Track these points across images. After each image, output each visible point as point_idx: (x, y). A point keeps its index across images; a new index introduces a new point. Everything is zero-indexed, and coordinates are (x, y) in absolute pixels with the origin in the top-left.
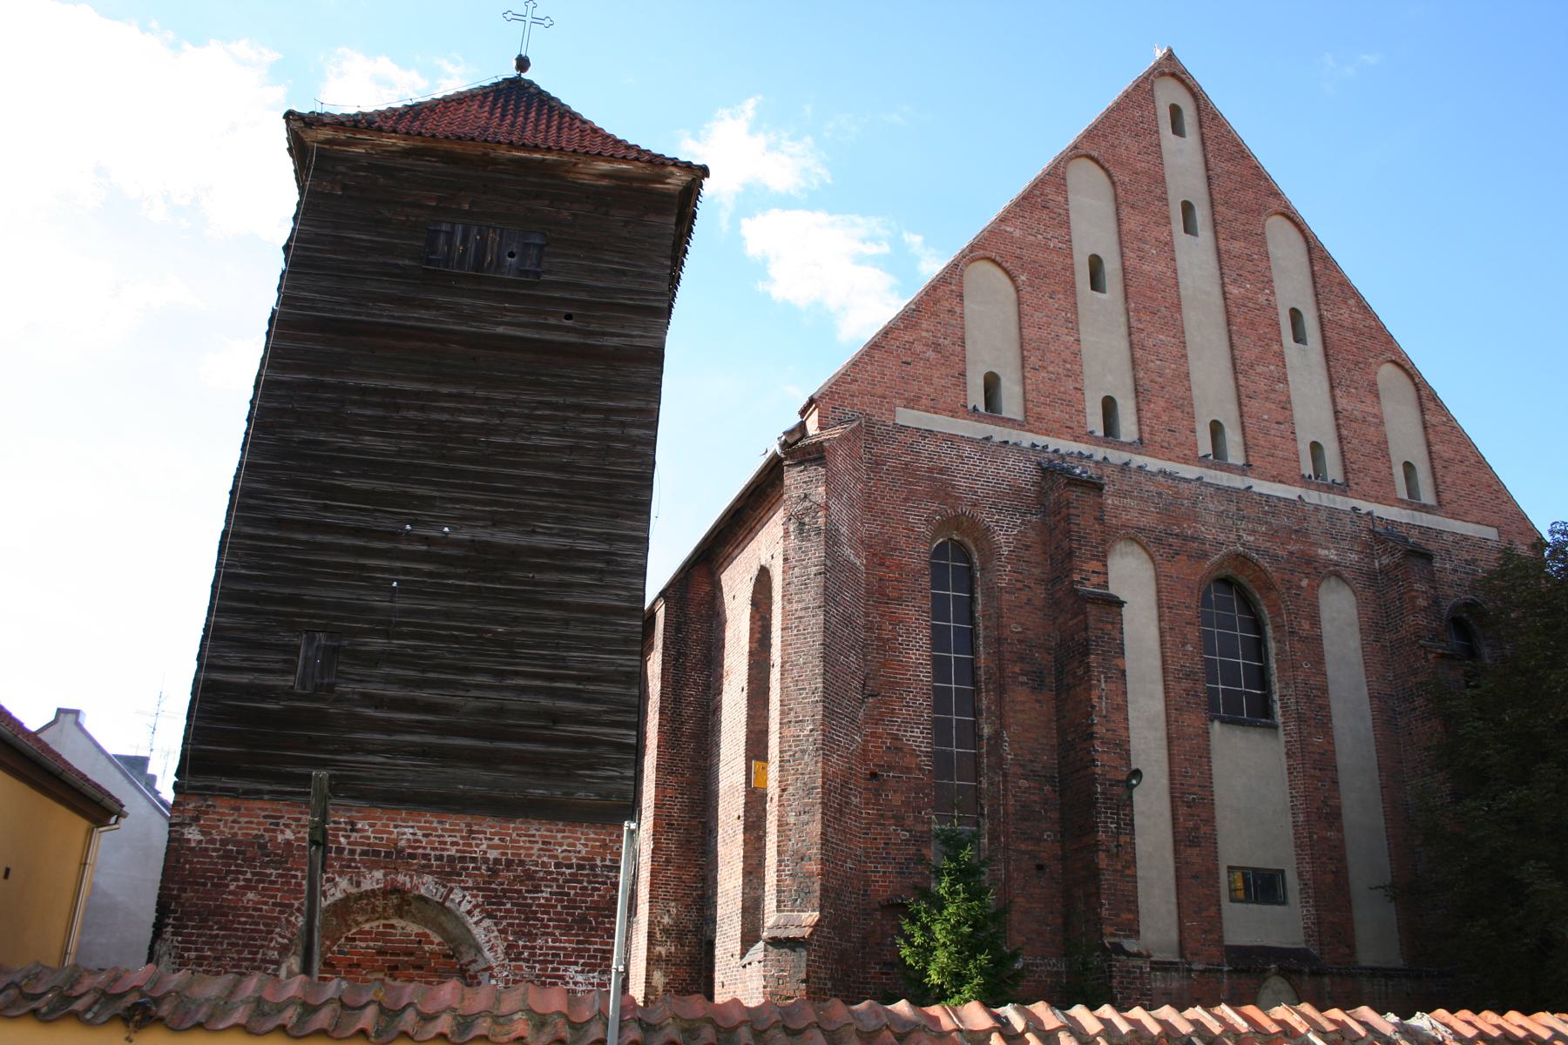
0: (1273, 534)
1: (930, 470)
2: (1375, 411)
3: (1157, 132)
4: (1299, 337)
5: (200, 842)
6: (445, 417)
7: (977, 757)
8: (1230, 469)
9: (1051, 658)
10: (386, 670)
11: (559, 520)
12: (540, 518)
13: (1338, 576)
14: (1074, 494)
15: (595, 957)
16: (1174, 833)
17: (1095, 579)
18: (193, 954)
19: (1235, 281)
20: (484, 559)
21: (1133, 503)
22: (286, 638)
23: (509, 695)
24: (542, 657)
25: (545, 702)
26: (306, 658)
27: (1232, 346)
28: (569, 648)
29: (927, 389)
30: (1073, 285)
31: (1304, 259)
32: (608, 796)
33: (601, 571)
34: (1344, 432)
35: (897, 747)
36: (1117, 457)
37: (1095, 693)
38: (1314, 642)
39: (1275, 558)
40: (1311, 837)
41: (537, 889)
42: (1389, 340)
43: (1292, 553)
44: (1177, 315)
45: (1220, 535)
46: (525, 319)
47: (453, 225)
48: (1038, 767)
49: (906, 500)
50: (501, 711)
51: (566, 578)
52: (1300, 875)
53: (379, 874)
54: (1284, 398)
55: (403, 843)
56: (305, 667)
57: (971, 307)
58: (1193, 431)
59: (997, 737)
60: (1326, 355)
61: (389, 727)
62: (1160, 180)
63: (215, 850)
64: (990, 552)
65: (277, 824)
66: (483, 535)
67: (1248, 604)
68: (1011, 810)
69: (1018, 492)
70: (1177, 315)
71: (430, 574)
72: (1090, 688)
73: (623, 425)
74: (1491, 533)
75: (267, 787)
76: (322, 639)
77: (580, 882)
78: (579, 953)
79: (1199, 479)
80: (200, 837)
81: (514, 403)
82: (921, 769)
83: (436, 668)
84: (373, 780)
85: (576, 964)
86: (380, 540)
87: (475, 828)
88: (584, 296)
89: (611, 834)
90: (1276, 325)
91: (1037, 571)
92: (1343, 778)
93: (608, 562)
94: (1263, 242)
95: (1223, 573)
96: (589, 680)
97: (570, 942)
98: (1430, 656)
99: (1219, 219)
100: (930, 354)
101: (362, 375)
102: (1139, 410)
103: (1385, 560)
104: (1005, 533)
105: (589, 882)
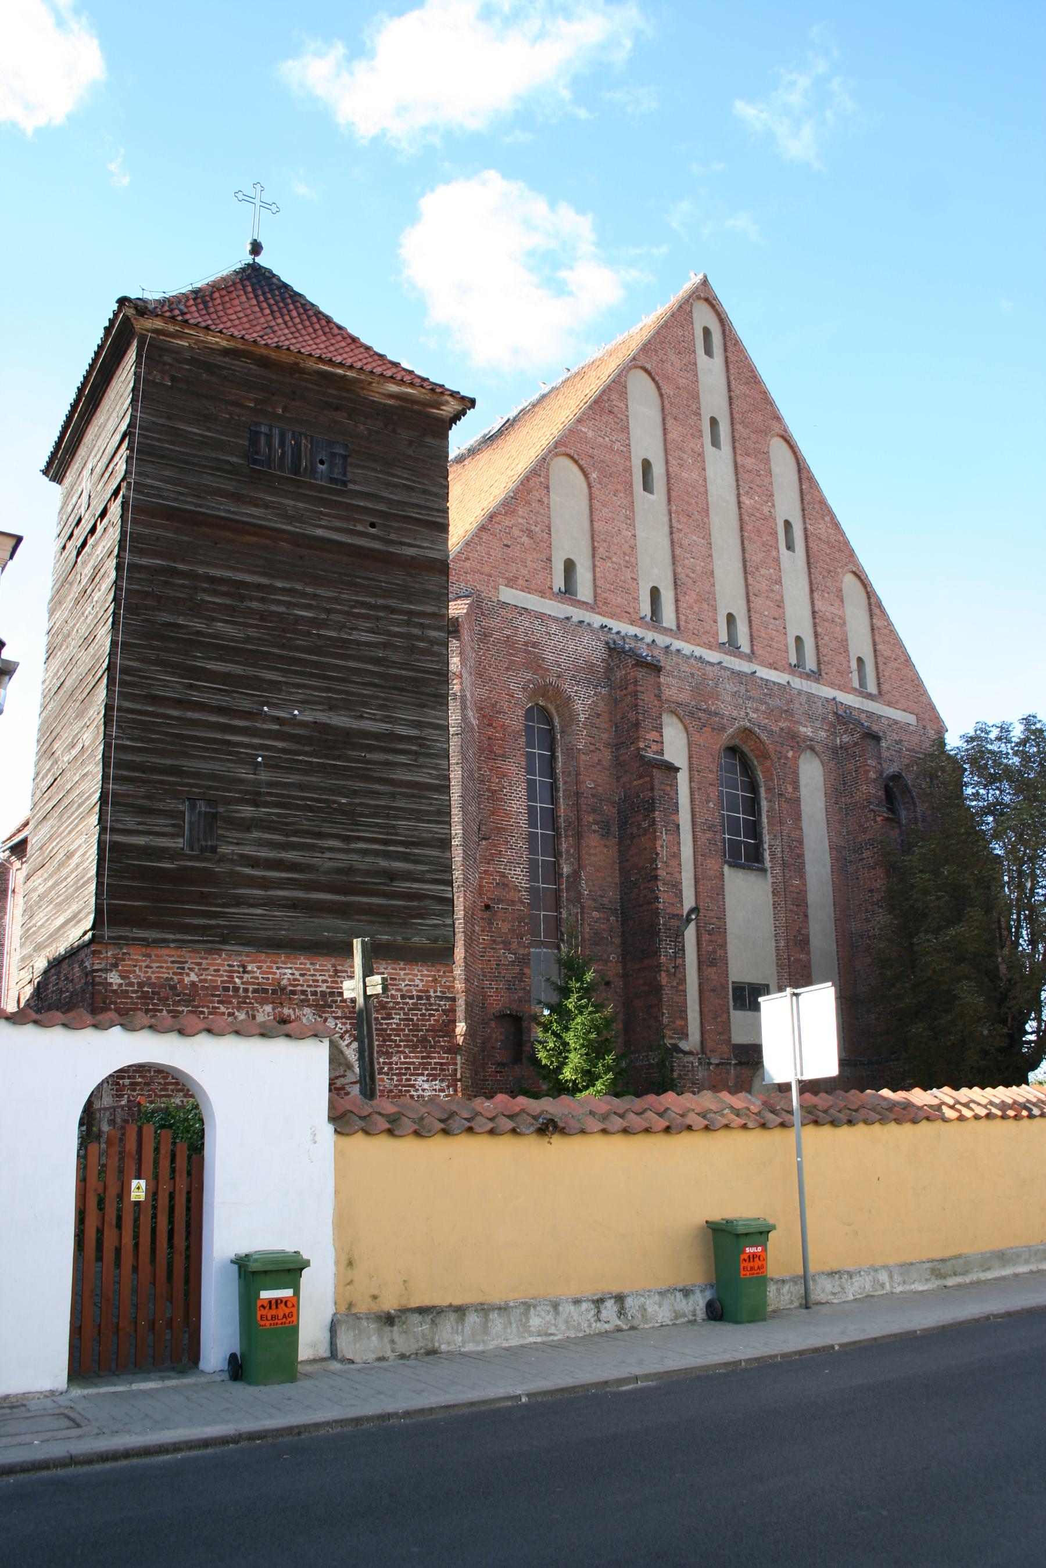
0: (770, 713)
1: (526, 644)
2: (840, 613)
3: (694, 352)
4: (647, 487)
5: (121, 985)
6: (281, 609)
7: (557, 892)
8: (740, 655)
9: (615, 810)
10: (255, 834)
11: (381, 707)
12: (365, 705)
14: (640, 673)
15: (435, 1069)
16: (699, 956)
17: (655, 747)
18: (127, 1081)
19: (747, 493)
21: (674, 681)
22: (172, 804)
23: (355, 857)
24: (377, 825)
25: (383, 863)
26: (190, 823)
27: (744, 550)
30: (631, 486)
31: (795, 478)
32: (435, 941)
33: (416, 753)
34: (819, 630)
36: (662, 640)
37: (659, 843)
38: (795, 802)
39: (771, 733)
40: (789, 959)
41: (389, 1017)
42: (852, 553)
43: (782, 729)
44: (705, 519)
45: (736, 712)
46: (337, 523)
47: (271, 428)
48: (606, 901)
49: (508, 669)
50: (350, 871)
51: (390, 757)
53: (268, 1008)
54: (778, 598)
55: (285, 982)
56: (191, 830)
57: (556, 498)
58: (715, 622)
59: (575, 875)
60: (809, 563)
61: (265, 884)
62: (695, 397)
63: (134, 992)
64: (570, 718)
65: (183, 968)
66: (323, 717)
67: (747, 769)
68: (587, 936)
69: (591, 667)
70: (705, 519)
71: (284, 751)
72: (655, 838)
73: (422, 626)
74: (911, 719)
75: (171, 937)
76: (202, 807)
77: (420, 1010)
78: (424, 1066)
79: (720, 663)
80: (120, 981)
81: (336, 600)
82: (522, 902)
83: (296, 833)
84: (257, 929)
85: (422, 1074)
86: (240, 718)
87: (339, 968)
88: (381, 507)
89: (439, 971)
91: (604, 736)
92: (811, 912)
93: (420, 746)
94: (768, 461)
95: (733, 743)
97: (417, 1058)
98: (879, 819)
99: (737, 435)
100: (525, 539)
101: (208, 564)
102: (677, 601)
103: (846, 738)
104: (583, 701)
105: (427, 1010)
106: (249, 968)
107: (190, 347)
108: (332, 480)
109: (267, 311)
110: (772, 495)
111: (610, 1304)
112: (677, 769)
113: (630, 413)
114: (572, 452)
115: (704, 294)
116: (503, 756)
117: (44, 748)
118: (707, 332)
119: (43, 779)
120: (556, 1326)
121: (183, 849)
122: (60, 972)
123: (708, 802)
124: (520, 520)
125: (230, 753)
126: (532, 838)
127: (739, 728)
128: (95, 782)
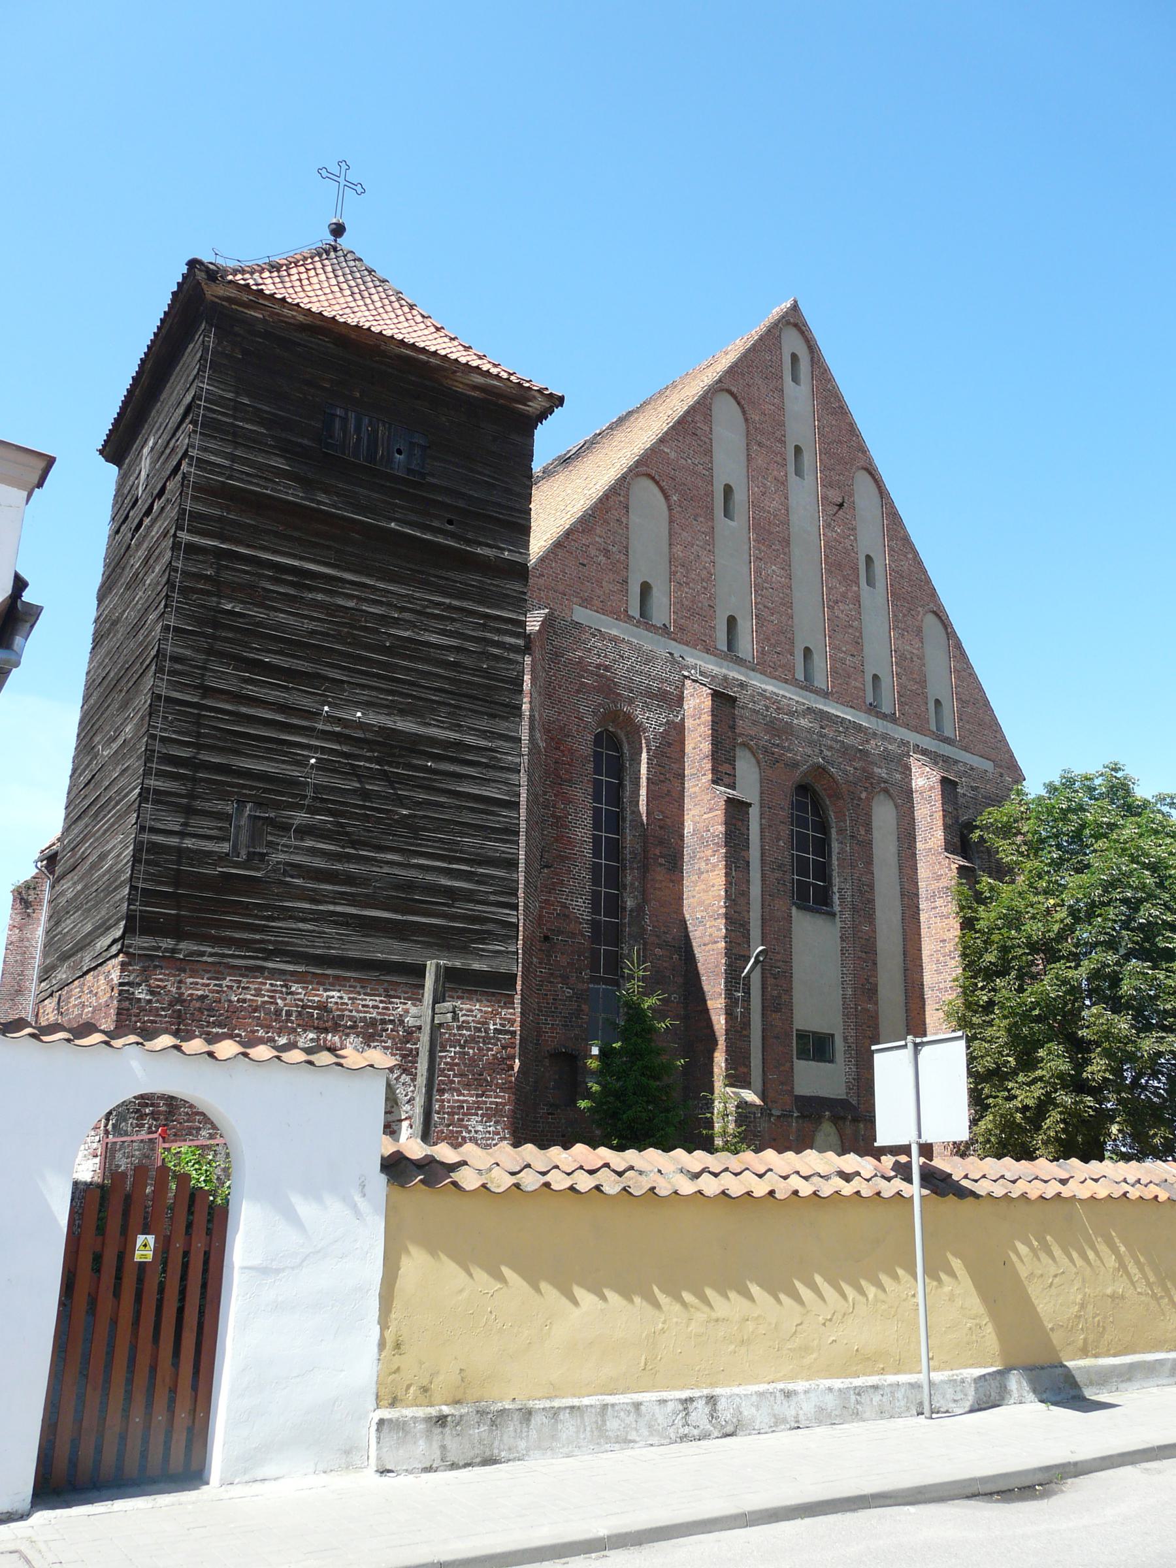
1: (598, 666)
3: (781, 377)
10: (309, 843)
13: (886, 791)
20: (390, 745)
22: (219, 806)
24: (441, 840)
28: (462, 834)
29: (599, 592)
33: (486, 766)
35: (565, 916)
42: (933, 594)
46: (413, 517)
48: (669, 938)
49: (578, 691)
52: (845, 1039)
57: (634, 519)
59: (640, 909)
67: (818, 808)
75: (209, 950)
82: (583, 935)
85: (477, 1115)
88: (461, 504)
90: (856, 569)
96: (480, 864)
100: (602, 559)
106: (293, 989)
107: (264, 319)
108: (410, 471)
109: (348, 292)
110: (854, 529)
111: (700, 1404)
112: (750, 805)
113: (714, 437)
114: (653, 473)
115: (793, 320)
116: (570, 781)
117: (84, 743)
118: (794, 358)
119: (80, 775)
120: (637, 1430)
121: (227, 854)
122: (84, 984)
123: (778, 840)
124: (597, 539)
125: (286, 754)
126: (596, 868)
127: (811, 766)
128: (135, 777)
